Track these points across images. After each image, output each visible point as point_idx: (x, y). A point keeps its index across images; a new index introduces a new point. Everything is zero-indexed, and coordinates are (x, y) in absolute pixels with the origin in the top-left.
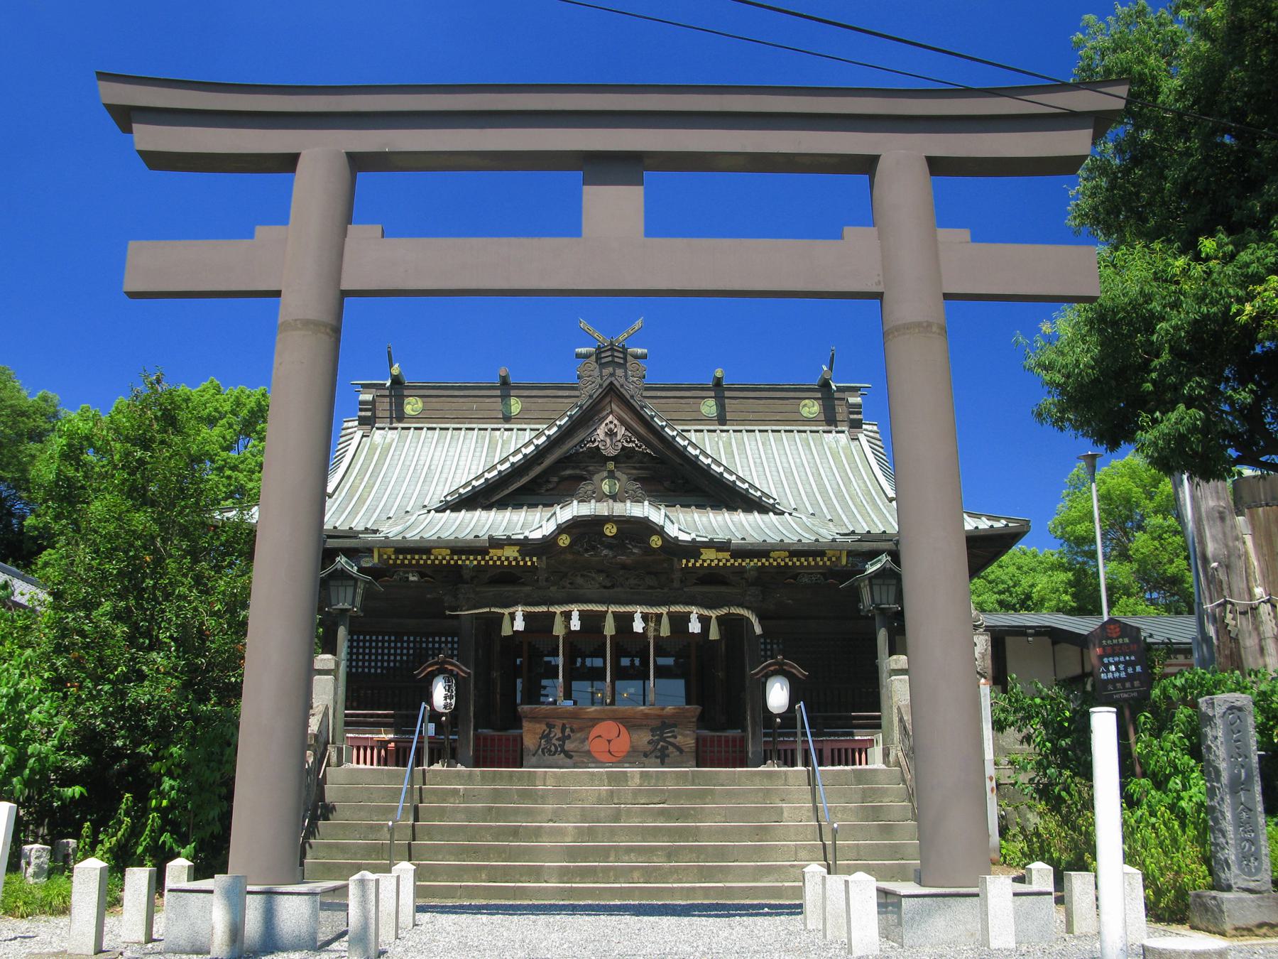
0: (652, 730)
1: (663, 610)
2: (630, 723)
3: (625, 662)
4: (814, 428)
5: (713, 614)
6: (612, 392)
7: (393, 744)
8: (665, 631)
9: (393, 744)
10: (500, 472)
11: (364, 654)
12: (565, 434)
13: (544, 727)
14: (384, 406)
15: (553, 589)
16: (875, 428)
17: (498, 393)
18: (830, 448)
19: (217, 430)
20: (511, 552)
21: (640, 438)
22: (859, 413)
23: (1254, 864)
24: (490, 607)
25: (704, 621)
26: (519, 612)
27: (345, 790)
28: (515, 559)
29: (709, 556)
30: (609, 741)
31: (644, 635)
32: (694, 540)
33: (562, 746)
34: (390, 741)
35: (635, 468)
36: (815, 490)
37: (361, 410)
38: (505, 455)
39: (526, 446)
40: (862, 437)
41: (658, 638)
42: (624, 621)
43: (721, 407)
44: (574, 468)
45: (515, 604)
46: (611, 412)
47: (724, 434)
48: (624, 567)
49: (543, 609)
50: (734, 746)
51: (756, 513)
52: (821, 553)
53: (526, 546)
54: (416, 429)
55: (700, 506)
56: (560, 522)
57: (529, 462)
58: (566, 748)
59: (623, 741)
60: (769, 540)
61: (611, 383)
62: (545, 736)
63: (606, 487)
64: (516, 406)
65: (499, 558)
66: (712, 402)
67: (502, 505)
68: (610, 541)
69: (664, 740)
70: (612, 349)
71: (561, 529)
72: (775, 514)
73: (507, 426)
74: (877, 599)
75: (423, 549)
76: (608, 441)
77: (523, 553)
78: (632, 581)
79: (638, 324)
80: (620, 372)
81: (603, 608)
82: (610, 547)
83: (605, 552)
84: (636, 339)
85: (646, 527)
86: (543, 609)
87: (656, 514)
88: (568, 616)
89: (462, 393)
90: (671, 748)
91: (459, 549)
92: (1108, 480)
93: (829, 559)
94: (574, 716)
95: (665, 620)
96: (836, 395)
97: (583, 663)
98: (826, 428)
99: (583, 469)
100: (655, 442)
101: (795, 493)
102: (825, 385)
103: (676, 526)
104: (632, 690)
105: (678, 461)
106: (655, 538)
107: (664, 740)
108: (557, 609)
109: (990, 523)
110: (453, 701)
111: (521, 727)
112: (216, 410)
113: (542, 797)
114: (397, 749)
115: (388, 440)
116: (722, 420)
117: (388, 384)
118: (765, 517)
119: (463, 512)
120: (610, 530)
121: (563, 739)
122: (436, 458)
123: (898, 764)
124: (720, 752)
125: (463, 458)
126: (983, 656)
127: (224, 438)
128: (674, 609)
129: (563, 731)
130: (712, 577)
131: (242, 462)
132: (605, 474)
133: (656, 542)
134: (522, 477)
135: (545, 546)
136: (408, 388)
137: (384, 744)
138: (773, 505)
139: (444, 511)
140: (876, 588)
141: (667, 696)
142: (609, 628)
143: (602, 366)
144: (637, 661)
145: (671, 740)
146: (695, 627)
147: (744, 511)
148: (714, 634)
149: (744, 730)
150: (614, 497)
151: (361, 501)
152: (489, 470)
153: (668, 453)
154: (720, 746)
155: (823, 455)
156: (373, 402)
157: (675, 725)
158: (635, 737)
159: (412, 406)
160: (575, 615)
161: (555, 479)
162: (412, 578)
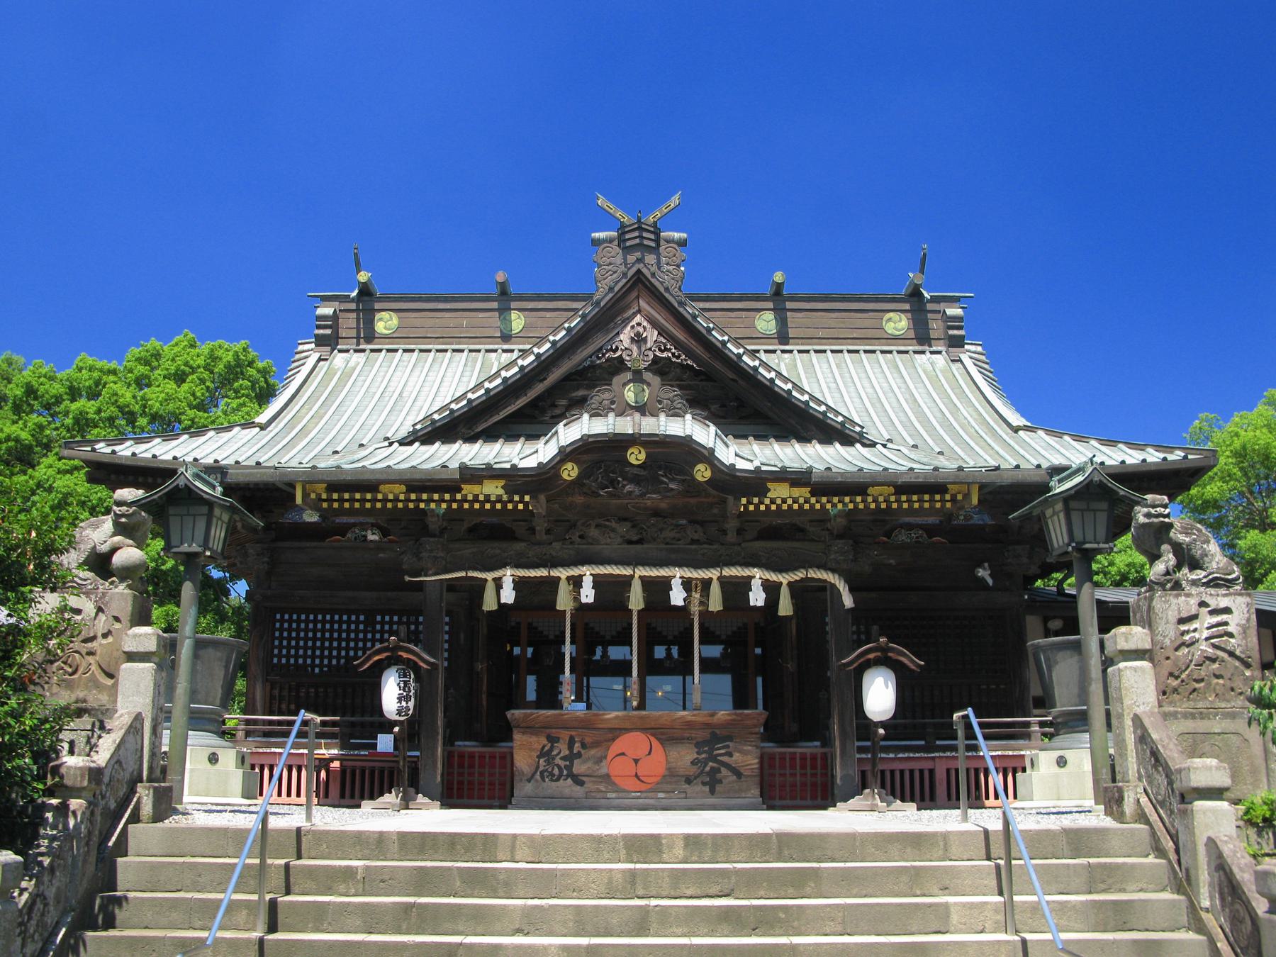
0: (697, 745)
1: (713, 574)
2: (666, 735)
3: (660, 652)
5: (784, 579)
6: (639, 283)
7: (336, 764)
8: (716, 604)
9: (336, 764)
11: (356, 640)
12: (577, 340)
13: (544, 741)
14: (348, 324)
15: (557, 545)
16: (979, 349)
17: (495, 305)
18: (925, 372)
19: (185, 387)
20: (493, 489)
21: (678, 344)
22: (960, 328)
24: (466, 570)
25: (771, 590)
26: (508, 576)
27: (154, 866)
28: (499, 500)
29: (779, 491)
30: (636, 761)
31: (684, 610)
32: (758, 468)
33: (569, 768)
34: (332, 760)
36: (913, 418)
37: (319, 327)
40: (965, 358)
41: (705, 614)
42: (657, 589)
43: (782, 322)
45: (503, 565)
46: (639, 311)
47: (786, 355)
48: (657, 513)
49: (542, 572)
50: (814, 767)
51: (837, 445)
53: (514, 478)
54: (389, 351)
55: (760, 437)
56: (563, 443)
58: (575, 770)
59: (657, 761)
61: (639, 271)
62: (545, 754)
63: (630, 395)
64: (517, 322)
66: (770, 316)
67: (490, 435)
68: (635, 471)
69: (713, 758)
70: (640, 229)
71: (566, 455)
72: (864, 445)
73: (506, 347)
74: (1078, 535)
75: (365, 484)
76: (635, 349)
77: (509, 490)
78: (669, 534)
79: (675, 201)
80: (651, 259)
81: (626, 571)
82: (636, 480)
83: (629, 488)
84: (673, 219)
86: (542, 572)
88: (577, 582)
89: (448, 306)
92: (1242, 433)
94: (585, 724)
95: (715, 589)
96: (930, 307)
97: (605, 653)
100: (699, 350)
101: (888, 423)
102: (915, 294)
104: (668, 688)
105: (731, 375)
106: (701, 467)
107: (713, 758)
108: (562, 573)
109: (1162, 455)
110: (411, 704)
111: (510, 739)
112: (186, 364)
113: (507, 884)
114: (343, 770)
115: (352, 364)
116: (783, 337)
117: (354, 294)
118: (850, 449)
119: (437, 444)
120: (636, 456)
121: (571, 757)
122: (410, 384)
123: (1142, 817)
124: (794, 775)
125: (445, 384)
126: (1245, 630)
127: (193, 395)
128: (727, 572)
129: (571, 747)
131: (213, 422)
132: (629, 375)
133: (702, 473)
134: (518, 398)
135: (543, 479)
136: (380, 300)
137: (325, 763)
138: (861, 434)
139: (411, 443)
140: (1076, 517)
141: (708, 695)
142: (636, 600)
143: (627, 250)
144: (675, 651)
145: (725, 759)
146: (757, 598)
147: (820, 443)
148: (785, 607)
149: (827, 742)
150: (642, 409)
151: (304, 431)
153: (718, 365)
154: (793, 766)
156: (335, 317)
157: (730, 738)
159: (385, 323)
160: (588, 582)
161: (564, 402)
162: (371, 537)
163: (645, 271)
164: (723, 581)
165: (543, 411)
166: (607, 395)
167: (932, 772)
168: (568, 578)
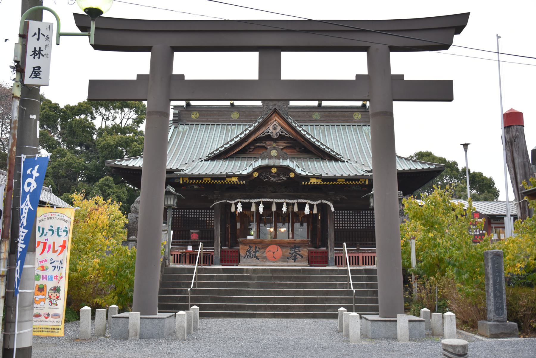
1: (295, 201)
4: (359, 124)
5: (315, 203)
10: (230, 145)
13: (248, 247)
20: (235, 179)
23: (501, 311)
25: (311, 207)
28: (236, 181)
29: (313, 181)
35: (285, 143)
38: (232, 138)
39: (241, 134)
44: (260, 143)
49: (247, 201)
52: (358, 180)
57: (242, 141)
60: (352, 175)
62: (248, 251)
65: (230, 181)
67: (232, 158)
68: (274, 174)
69: (295, 252)
71: (255, 170)
72: (341, 162)
75: (200, 178)
81: (271, 200)
82: (274, 177)
85: (288, 170)
86: (247, 201)
87: (292, 164)
90: (298, 256)
91: (214, 178)
93: (361, 182)
98: (364, 124)
99: (265, 143)
100: (293, 132)
103: (300, 169)
105: (303, 140)
106: (292, 173)
108: (253, 201)
109: (428, 166)
115: (185, 130)
118: (337, 163)
121: (256, 252)
125: (216, 137)
128: (300, 201)
129: (256, 249)
130: (315, 187)
138: (340, 158)
142: (274, 208)
149: (327, 249)
152: (226, 144)
155: (362, 136)
158: (284, 250)
161: (253, 147)
163: (277, 108)
164: (297, 203)
165: (247, 150)
166: (266, 154)
167: (358, 257)
168: (255, 203)
